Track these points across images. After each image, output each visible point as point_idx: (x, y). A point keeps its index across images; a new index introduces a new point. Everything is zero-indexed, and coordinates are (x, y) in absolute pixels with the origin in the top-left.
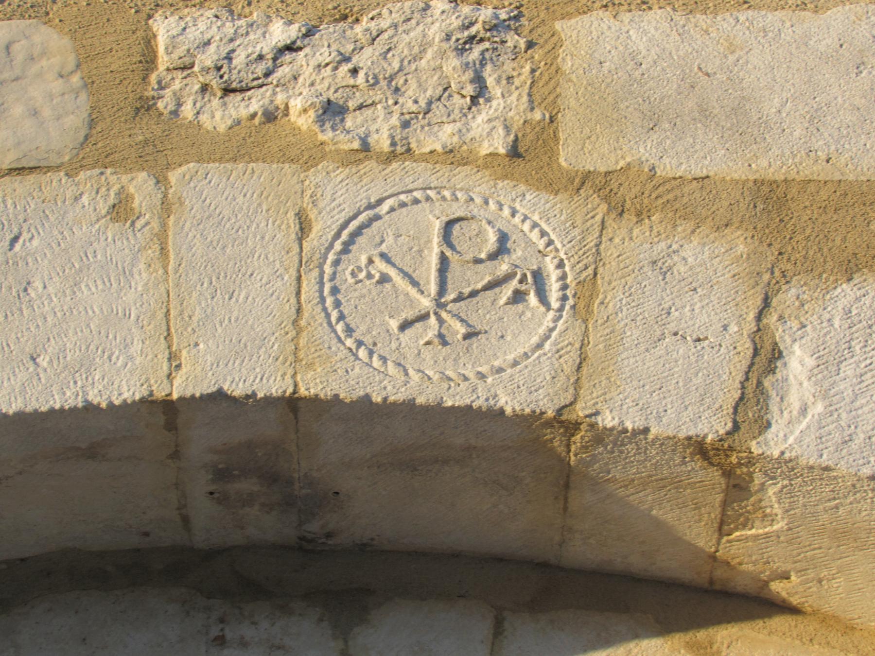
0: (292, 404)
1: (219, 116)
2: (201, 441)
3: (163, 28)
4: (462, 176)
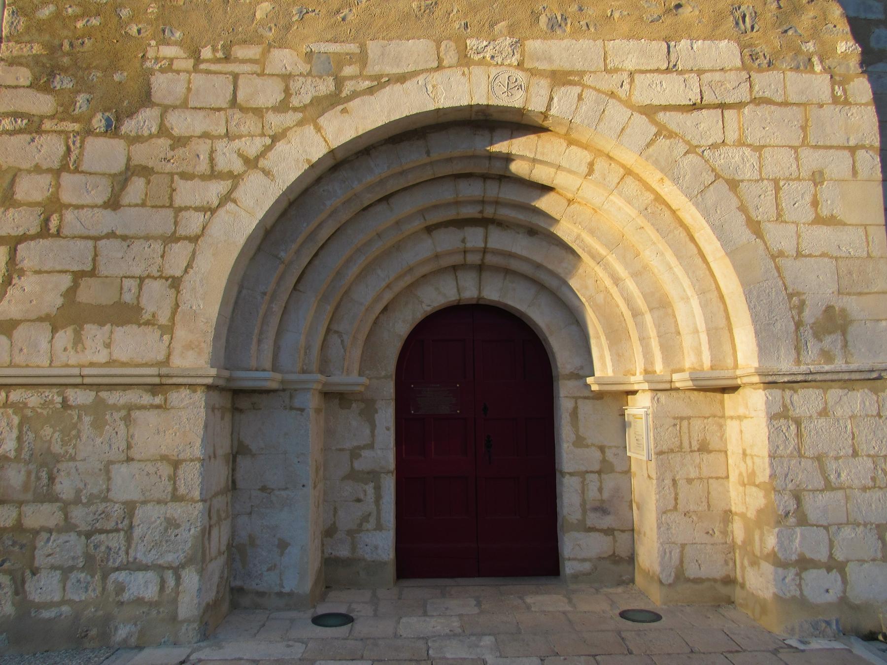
0: (488, 105)
1: (477, 58)
2: (474, 109)
3: (468, 42)
4: (511, 69)
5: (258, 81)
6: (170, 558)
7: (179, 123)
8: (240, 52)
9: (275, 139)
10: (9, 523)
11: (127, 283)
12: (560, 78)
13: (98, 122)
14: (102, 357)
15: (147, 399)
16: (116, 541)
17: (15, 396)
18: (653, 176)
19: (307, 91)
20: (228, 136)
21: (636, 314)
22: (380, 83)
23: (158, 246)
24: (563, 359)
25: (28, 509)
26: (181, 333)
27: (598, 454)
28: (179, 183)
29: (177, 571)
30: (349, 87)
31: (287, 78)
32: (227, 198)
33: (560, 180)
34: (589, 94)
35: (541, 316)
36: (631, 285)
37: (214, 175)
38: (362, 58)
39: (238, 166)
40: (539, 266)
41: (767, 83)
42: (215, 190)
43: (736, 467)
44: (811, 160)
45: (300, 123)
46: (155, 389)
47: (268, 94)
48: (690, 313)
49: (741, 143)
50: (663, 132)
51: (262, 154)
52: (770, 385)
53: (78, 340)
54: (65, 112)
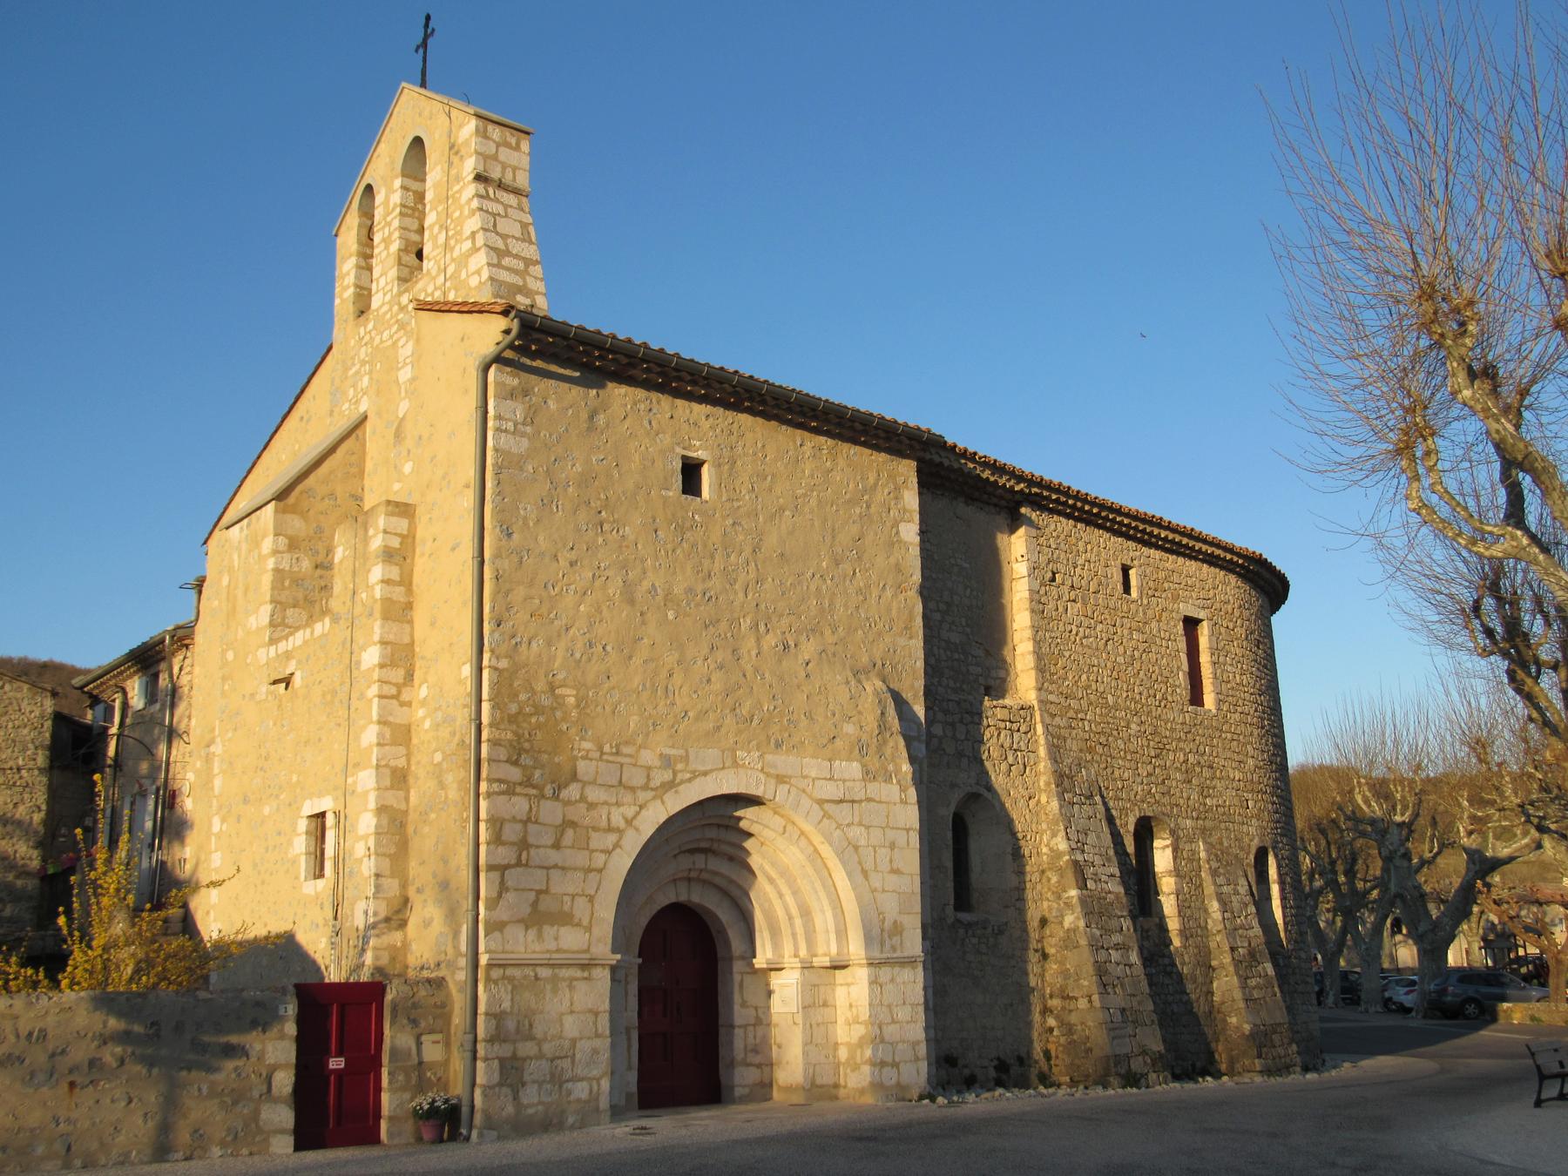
5: (634, 770)
6: (595, 1073)
7: (594, 794)
8: (626, 750)
9: (641, 807)
10: (509, 1054)
11: (566, 898)
12: (781, 779)
13: (548, 791)
14: (553, 946)
15: (579, 973)
16: (566, 1064)
17: (509, 972)
18: (817, 839)
19: (660, 777)
20: (618, 804)
21: (790, 918)
22: (695, 774)
23: (580, 875)
24: (737, 946)
25: (520, 1045)
26: (596, 931)
27: (753, 1012)
28: (593, 835)
29: (598, 1080)
30: (679, 777)
31: (649, 768)
32: (617, 845)
33: (767, 833)
34: (793, 790)
35: (724, 915)
36: (789, 899)
37: (610, 829)
38: (686, 759)
39: (622, 825)
40: (732, 881)
41: (874, 789)
42: (611, 838)
43: (842, 1014)
44: (890, 834)
45: (654, 798)
46: (584, 967)
47: (638, 779)
48: (824, 919)
49: (860, 824)
50: (826, 815)
51: (634, 817)
52: (870, 965)
53: (540, 936)
54: (528, 782)
